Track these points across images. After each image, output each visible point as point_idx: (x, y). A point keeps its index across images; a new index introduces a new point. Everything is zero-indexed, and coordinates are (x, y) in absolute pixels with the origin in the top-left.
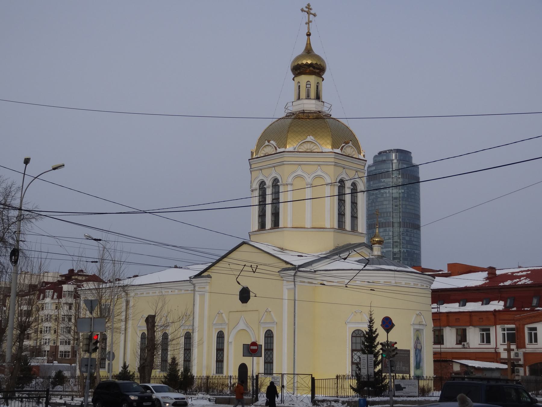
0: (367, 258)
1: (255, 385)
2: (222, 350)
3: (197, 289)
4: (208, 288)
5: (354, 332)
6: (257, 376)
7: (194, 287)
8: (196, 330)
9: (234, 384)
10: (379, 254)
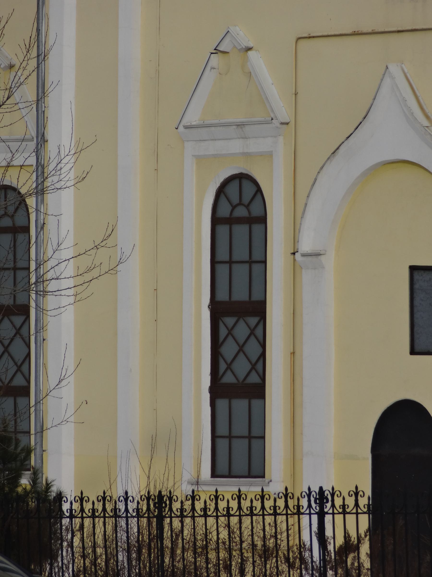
8: (65, 172)
9: (349, 547)
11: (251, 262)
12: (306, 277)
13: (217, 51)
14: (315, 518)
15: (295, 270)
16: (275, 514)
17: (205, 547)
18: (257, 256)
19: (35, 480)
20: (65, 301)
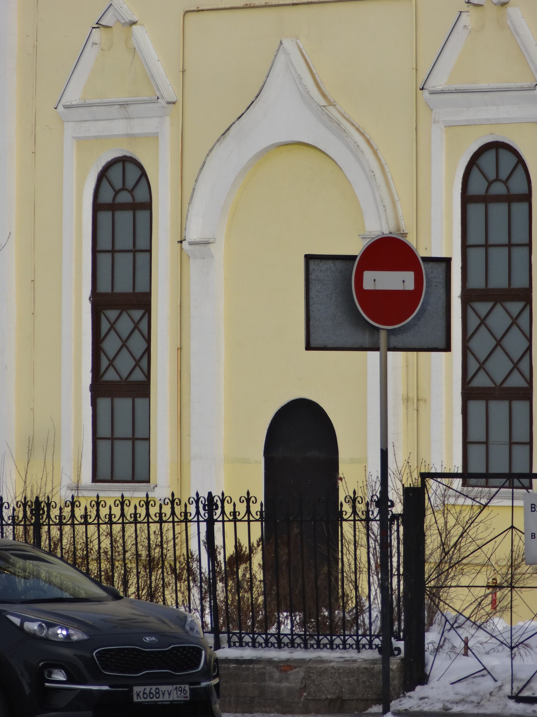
1: (395, 560)
6: (415, 497)
9: (240, 557)
12: (194, 267)
13: (99, 25)
14: (203, 526)
15: (182, 259)
16: (161, 521)
17: (86, 557)
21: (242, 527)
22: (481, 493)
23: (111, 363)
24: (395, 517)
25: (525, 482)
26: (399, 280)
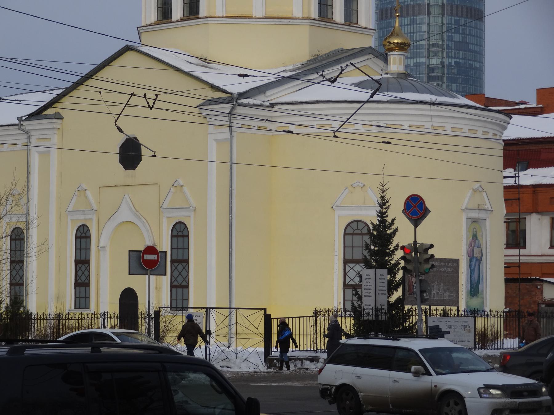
0: (377, 77)
2: (87, 262)
3: (33, 141)
4: (55, 140)
5: (349, 225)
6: (157, 313)
7: (29, 138)
8: (35, 223)
10: (401, 69)
11: (86, 249)
12: (101, 253)
13: (77, 190)
14: (102, 320)
15: (98, 251)
16: (91, 319)
17: (72, 328)
18: (185, 246)
19: (24, 309)
20: (34, 259)
21: (112, 320)
22: (174, 312)
23: (80, 278)
24: (152, 318)
25: (186, 309)
26: (153, 257)
